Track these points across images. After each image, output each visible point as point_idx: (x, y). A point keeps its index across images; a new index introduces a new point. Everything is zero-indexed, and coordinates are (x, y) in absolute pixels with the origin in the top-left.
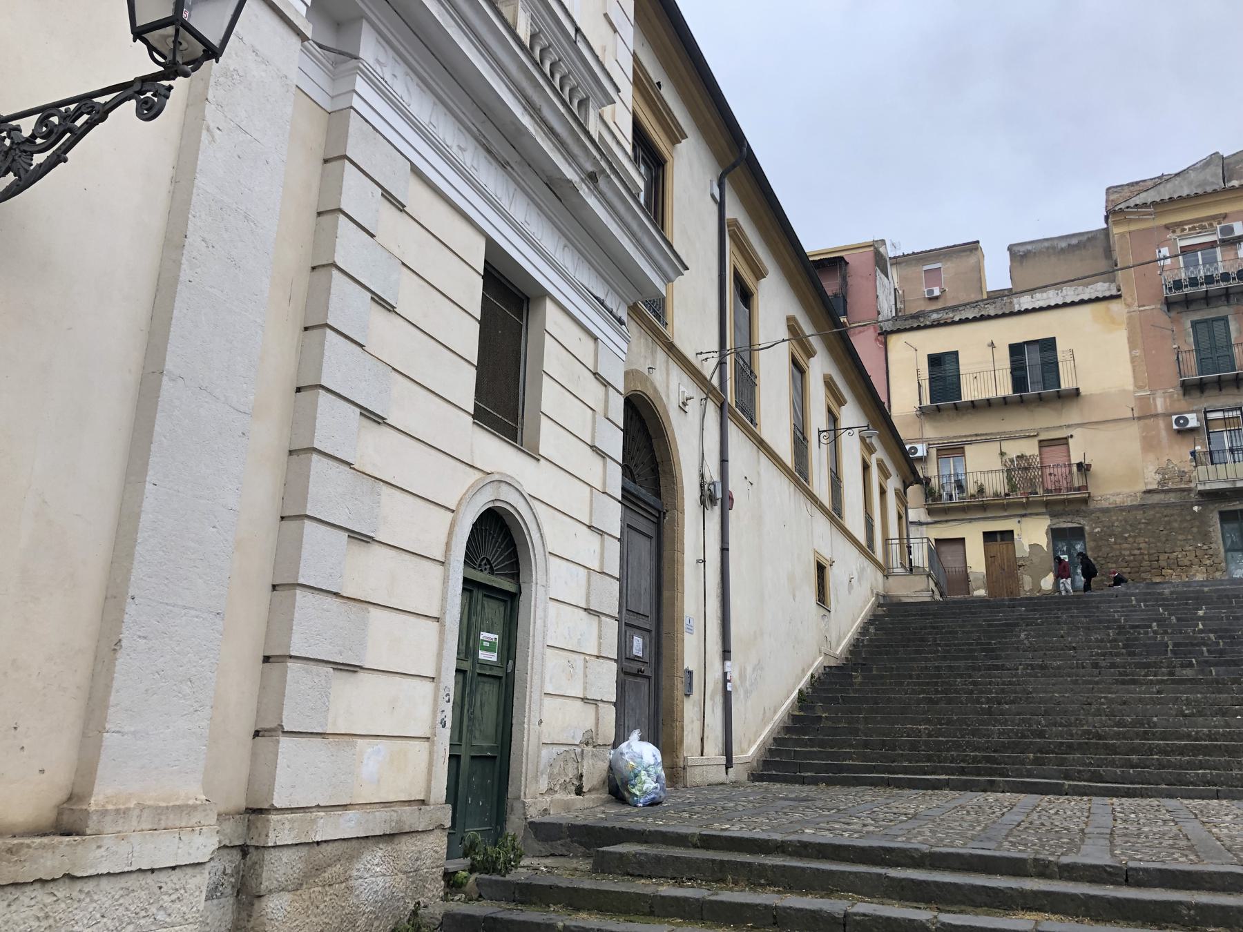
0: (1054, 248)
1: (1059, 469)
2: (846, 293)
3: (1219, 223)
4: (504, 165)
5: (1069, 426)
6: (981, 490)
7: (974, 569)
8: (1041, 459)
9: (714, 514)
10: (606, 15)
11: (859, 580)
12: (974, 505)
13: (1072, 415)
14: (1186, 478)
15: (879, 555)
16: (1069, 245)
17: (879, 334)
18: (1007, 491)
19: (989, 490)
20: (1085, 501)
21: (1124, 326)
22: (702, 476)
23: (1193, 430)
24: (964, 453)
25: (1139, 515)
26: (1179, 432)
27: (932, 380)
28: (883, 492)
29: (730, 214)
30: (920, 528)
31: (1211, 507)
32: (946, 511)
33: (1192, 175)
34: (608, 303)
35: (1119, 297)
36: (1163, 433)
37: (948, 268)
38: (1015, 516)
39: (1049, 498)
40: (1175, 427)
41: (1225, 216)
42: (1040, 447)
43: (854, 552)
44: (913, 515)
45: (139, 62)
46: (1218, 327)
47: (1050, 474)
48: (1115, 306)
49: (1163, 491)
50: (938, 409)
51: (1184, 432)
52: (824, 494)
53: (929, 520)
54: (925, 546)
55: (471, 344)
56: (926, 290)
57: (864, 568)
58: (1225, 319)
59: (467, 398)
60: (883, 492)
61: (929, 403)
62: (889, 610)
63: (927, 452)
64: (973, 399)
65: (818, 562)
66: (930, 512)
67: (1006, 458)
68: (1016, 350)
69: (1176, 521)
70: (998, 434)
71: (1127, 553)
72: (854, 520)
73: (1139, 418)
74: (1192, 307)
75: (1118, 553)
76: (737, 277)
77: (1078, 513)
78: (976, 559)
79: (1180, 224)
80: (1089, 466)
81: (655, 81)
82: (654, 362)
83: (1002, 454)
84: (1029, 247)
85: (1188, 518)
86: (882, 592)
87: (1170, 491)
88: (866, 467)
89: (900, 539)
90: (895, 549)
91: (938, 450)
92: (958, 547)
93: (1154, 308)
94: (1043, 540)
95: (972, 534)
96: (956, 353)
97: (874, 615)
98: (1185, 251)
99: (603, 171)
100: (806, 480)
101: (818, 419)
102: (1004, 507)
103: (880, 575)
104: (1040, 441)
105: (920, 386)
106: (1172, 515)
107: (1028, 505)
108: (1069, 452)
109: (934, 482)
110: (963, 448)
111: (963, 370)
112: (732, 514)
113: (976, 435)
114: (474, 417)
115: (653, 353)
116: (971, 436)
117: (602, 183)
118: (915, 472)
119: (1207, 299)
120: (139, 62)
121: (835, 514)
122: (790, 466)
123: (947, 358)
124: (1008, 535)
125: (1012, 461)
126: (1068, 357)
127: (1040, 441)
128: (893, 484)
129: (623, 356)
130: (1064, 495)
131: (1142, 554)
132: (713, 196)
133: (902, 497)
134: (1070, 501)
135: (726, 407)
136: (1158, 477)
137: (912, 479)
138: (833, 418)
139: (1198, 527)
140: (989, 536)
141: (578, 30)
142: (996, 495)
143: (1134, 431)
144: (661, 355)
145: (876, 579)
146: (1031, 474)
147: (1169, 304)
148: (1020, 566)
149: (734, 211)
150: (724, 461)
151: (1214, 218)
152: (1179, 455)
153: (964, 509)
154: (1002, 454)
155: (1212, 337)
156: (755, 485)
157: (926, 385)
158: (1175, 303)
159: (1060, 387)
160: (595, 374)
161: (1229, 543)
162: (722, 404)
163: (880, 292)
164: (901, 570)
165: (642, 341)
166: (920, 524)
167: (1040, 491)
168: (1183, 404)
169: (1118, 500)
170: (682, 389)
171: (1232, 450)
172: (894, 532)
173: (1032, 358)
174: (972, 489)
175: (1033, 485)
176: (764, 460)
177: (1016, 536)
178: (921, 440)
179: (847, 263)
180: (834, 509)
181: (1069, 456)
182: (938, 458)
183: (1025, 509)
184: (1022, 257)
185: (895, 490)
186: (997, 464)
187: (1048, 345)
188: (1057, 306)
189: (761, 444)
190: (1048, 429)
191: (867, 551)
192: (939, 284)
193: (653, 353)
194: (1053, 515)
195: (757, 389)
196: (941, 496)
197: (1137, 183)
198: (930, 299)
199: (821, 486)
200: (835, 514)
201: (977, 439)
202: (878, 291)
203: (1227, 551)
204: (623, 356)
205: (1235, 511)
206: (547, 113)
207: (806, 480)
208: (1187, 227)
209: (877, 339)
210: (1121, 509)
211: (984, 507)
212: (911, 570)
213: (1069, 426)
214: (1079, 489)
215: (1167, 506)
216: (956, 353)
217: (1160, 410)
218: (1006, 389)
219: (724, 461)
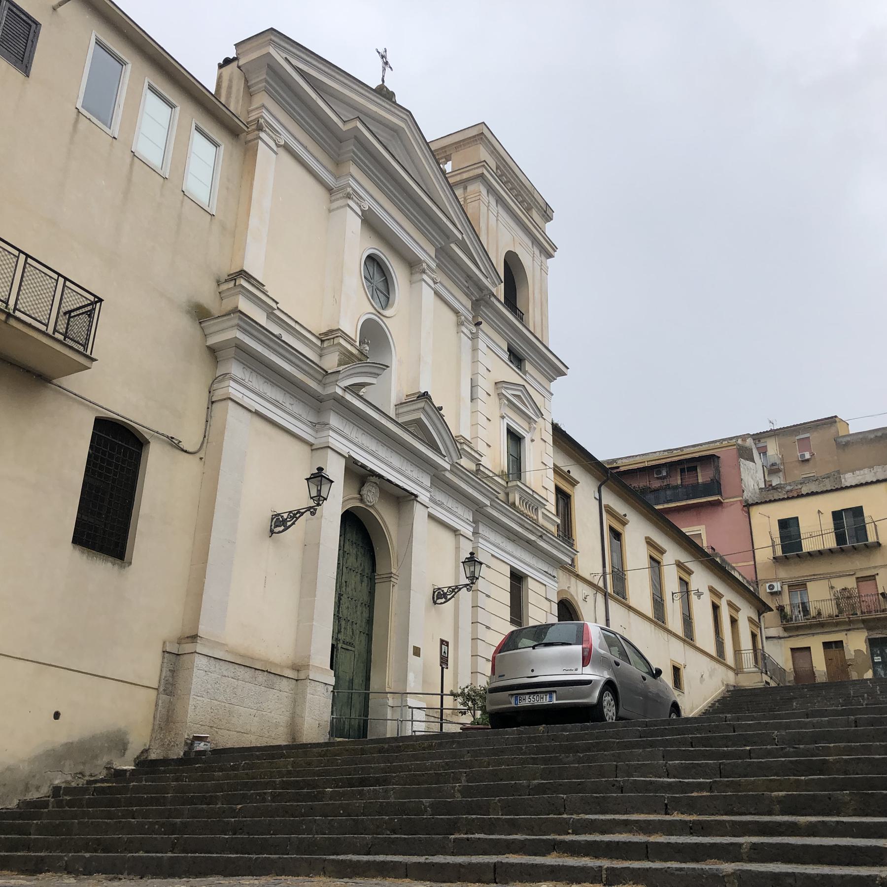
1: (869, 597)
4: (514, 541)
5: (875, 567)
6: (819, 614)
7: (818, 668)
8: (858, 590)
10: (542, 462)
11: (711, 676)
12: (829, 623)
13: (878, 559)
16: (876, 436)
17: (744, 506)
18: (837, 614)
24: (806, 587)
28: (734, 621)
30: (780, 641)
32: (798, 628)
34: (549, 572)
37: (815, 437)
38: (843, 630)
39: (863, 618)
42: (857, 582)
45: (467, 582)
47: (863, 601)
53: (786, 635)
55: (508, 601)
56: (799, 454)
57: (714, 669)
59: (508, 617)
60: (734, 621)
62: (732, 694)
63: (782, 587)
64: (809, 551)
65: (674, 666)
66: (786, 629)
67: (834, 590)
70: (828, 574)
76: (611, 529)
78: (819, 662)
81: (566, 471)
82: (570, 584)
83: (832, 588)
88: (715, 608)
91: (789, 586)
94: (863, 647)
95: (815, 644)
96: (797, 518)
99: (544, 534)
102: (837, 624)
104: (857, 578)
107: (850, 622)
108: (876, 585)
109: (788, 609)
110: (805, 584)
111: (803, 530)
113: (814, 575)
114: (510, 622)
115: (569, 579)
120: (467, 582)
122: (651, 617)
124: (839, 644)
127: (857, 578)
129: (556, 589)
130: (874, 615)
132: (595, 498)
134: (879, 619)
135: (607, 594)
138: (684, 583)
140: (827, 645)
141: (533, 491)
142: (830, 616)
144: (573, 580)
146: (852, 601)
148: (849, 665)
153: (810, 627)
156: (627, 629)
157: (778, 541)
159: (867, 541)
160: (546, 598)
162: (605, 594)
165: (564, 576)
166: (780, 638)
167: (859, 613)
170: (584, 592)
174: (813, 612)
175: (854, 608)
176: (632, 614)
177: (844, 645)
178: (776, 580)
179: (719, 457)
180: (686, 635)
181: (877, 588)
182: (789, 592)
183: (850, 625)
184: (844, 445)
185: (748, 618)
186: (827, 594)
187: (858, 512)
190: (861, 569)
192: (809, 449)
193: (569, 579)
194: (869, 629)
195: (626, 581)
198: (803, 461)
201: (815, 578)
202: (742, 475)
204: (556, 589)
206: (526, 525)
209: (742, 510)
211: (822, 625)
213: (875, 567)
216: (797, 518)
218: (830, 542)
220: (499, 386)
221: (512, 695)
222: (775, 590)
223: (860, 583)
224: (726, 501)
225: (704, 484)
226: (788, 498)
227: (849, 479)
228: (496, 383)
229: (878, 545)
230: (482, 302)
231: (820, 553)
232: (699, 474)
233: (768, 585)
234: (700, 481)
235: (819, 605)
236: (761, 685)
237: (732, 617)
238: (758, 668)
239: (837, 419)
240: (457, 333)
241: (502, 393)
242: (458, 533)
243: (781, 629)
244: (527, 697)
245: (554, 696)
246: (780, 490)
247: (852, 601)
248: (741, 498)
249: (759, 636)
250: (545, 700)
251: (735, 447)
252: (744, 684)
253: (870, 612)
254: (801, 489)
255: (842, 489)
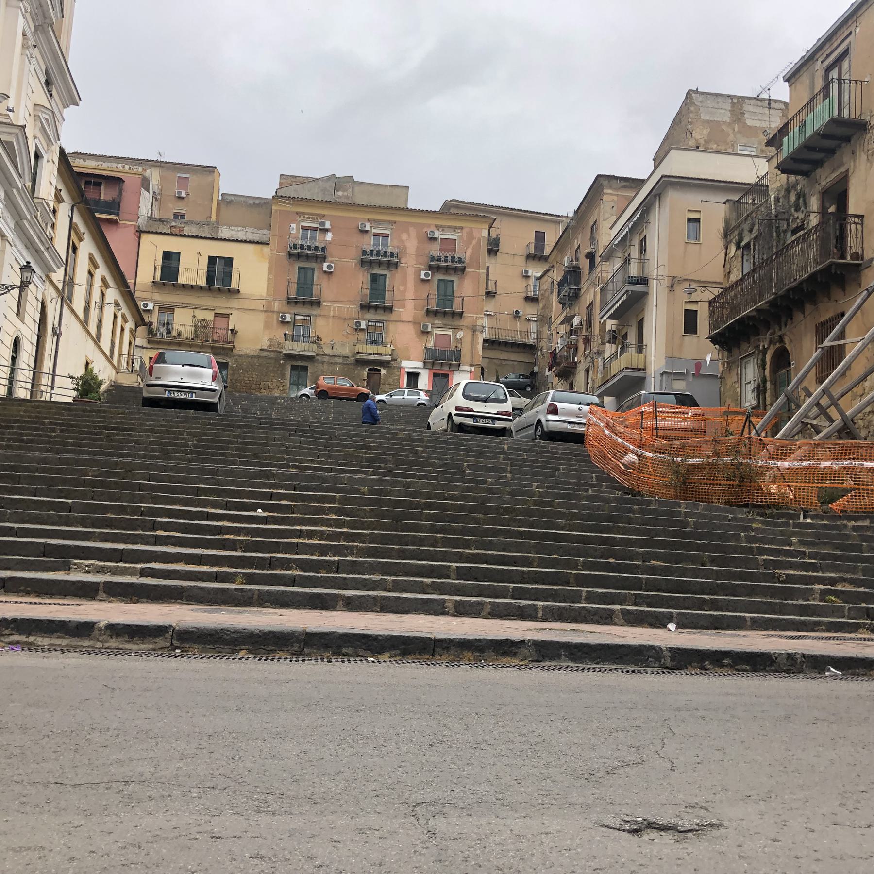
0: (245, 202)
2: (121, 201)
3: (321, 219)
5: (231, 308)
6: (179, 335)
9: (56, 337)
13: (234, 303)
14: (280, 346)
15: (115, 362)
16: (254, 203)
17: (137, 231)
19: (184, 335)
20: (231, 350)
21: (267, 261)
22: (54, 325)
23: (288, 322)
24: (174, 312)
25: (256, 361)
26: (282, 322)
27: (163, 267)
28: (122, 330)
29: (74, 220)
30: (142, 349)
31: (288, 362)
32: (159, 343)
33: (321, 183)
35: (269, 244)
36: (275, 322)
37: (194, 180)
40: (280, 320)
41: (324, 216)
42: (215, 316)
43: (103, 358)
44: (138, 342)
46: (309, 273)
47: (216, 332)
48: (266, 249)
49: (268, 351)
50: (164, 284)
51: (284, 323)
52: (93, 332)
53: (148, 346)
54: (139, 360)
58: (313, 269)
60: (122, 330)
61: (159, 280)
66: (149, 342)
67: (196, 319)
68: (212, 260)
69: (271, 366)
70: (194, 305)
71: (246, 379)
72: (106, 344)
73: (265, 311)
74: (300, 259)
75: (242, 378)
77: (227, 355)
79: (303, 213)
80: (237, 332)
83: (194, 316)
84: (233, 198)
85: (278, 366)
86: (113, 379)
87: (272, 351)
88: (115, 317)
89: (128, 355)
90: (124, 360)
91: (159, 308)
92: (444, 380)
93: (284, 254)
96: (179, 253)
97: (108, 390)
98: (304, 228)
100: (87, 325)
101: (96, 297)
102: (191, 346)
103: (114, 372)
104: (215, 313)
105: (155, 268)
106: (270, 363)
109: (155, 326)
110: (174, 309)
112: (61, 339)
113: (182, 303)
116: (179, 303)
117: (49, 249)
118: (142, 319)
119: (308, 257)
121: (97, 341)
123: (174, 255)
125: (198, 321)
126: (237, 272)
127: (215, 313)
128: (130, 325)
131: (253, 380)
132: (69, 215)
133: (133, 333)
134: (224, 348)
136: (268, 343)
137: (141, 323)
139: (281, 371)
142: (187, 338)
143: (262, 317)
145: (112, 373)
146: (207, 330)
147: (290, 255)
149: (77, 219)
150: (60, 319)
151: (319, 215)
152: (278, 333)
154: (194, 316)
155: (305, 277)
158: (293, 255)
160: (36, 298)
161: (292, 380)
163: (141, 203)
164: (126, 371)
166: (143, 347)
168: (286, 308)
169: (248, 351)
171: (303, 336)
172: (125, 351)
173: (219, 267)
178: (150, 300)
179: (124, 181)
180: (97, 338)
186: (190, 321)
187: (229, 262)
188: (241, 241)
189: (73, 311)
190: (221, 308)
191: (109, 359)
196: (157, 334)
197: (296, 177)
199: (93, 328)
200: (97, 341)
201: (183, 306)
203: (291, 384)
205: (298, 366)
207: (87, 325)
208: (306, 216)
209: (135, 234)
210: (248, 356)
211: (179, 344)
212: (132, 371)
213: (231, 308)
214: (229, 343)
215: (269, 358)
216: (179, 253)
217: (276, 309)
218: (202, 281)
219: (60, 319)
220: (38, 108)
221: (166, 390)
222: (148, 308)
223: (217, 318)
224: (122, 222)
225: (106, 202)
226: (171, 234)
227: (225, 233)
228: (35, 105)
229: (238, 291)
230: (40, 28)
231: (192, 286)
232: (102, 192)
233: (143, 303)
234: (102, 197)
235: (181, 328)
236: (135, 384)
237: (122, 327)
238: (128, 370)
239: (215, 170)
240: (22, 54)
241: (39, 116)
242: (5, 238)
243: (145, 340)
244: (176, 393)
245: (194, 395)
246: (165, 224)
247: (207, 330)
248: (135, 223)
249: (133, 344)
250: (188, 397)
251: (140, 176)
252: (122, 382)
253: (220, 341)
254: (183, 227)
255: (217, 239)
